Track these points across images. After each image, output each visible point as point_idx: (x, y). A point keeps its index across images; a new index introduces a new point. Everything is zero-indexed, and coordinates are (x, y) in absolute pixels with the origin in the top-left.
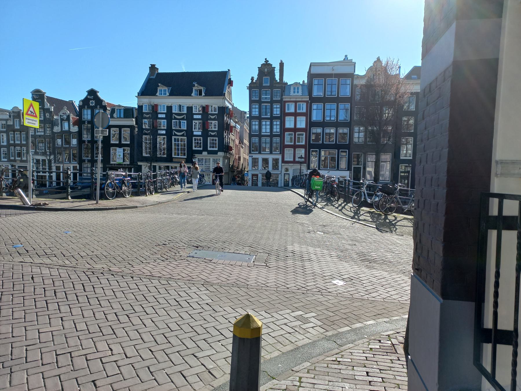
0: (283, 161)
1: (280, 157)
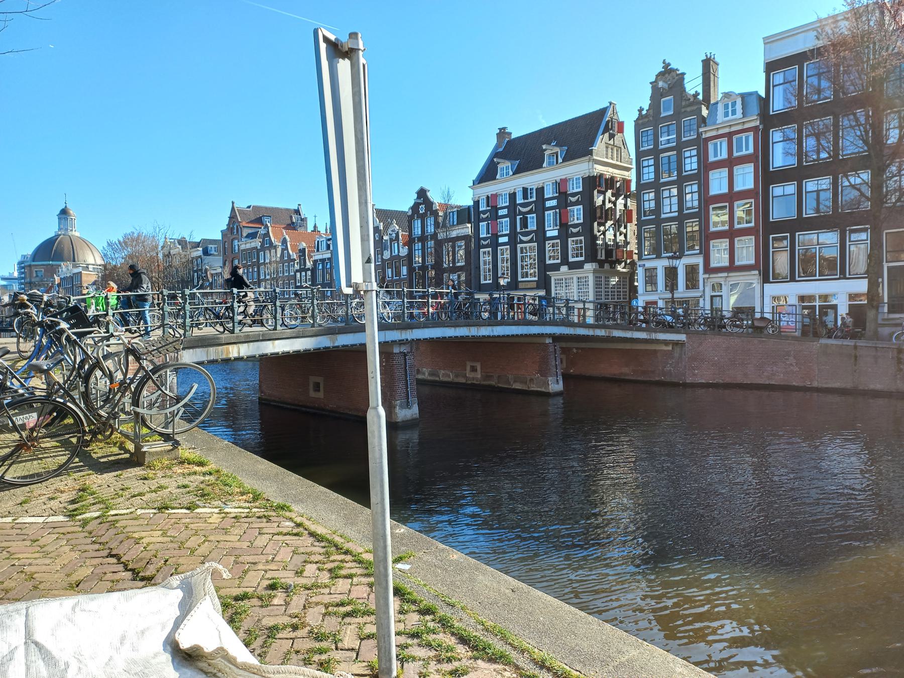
0: (708, 270)
1: (699, 260)
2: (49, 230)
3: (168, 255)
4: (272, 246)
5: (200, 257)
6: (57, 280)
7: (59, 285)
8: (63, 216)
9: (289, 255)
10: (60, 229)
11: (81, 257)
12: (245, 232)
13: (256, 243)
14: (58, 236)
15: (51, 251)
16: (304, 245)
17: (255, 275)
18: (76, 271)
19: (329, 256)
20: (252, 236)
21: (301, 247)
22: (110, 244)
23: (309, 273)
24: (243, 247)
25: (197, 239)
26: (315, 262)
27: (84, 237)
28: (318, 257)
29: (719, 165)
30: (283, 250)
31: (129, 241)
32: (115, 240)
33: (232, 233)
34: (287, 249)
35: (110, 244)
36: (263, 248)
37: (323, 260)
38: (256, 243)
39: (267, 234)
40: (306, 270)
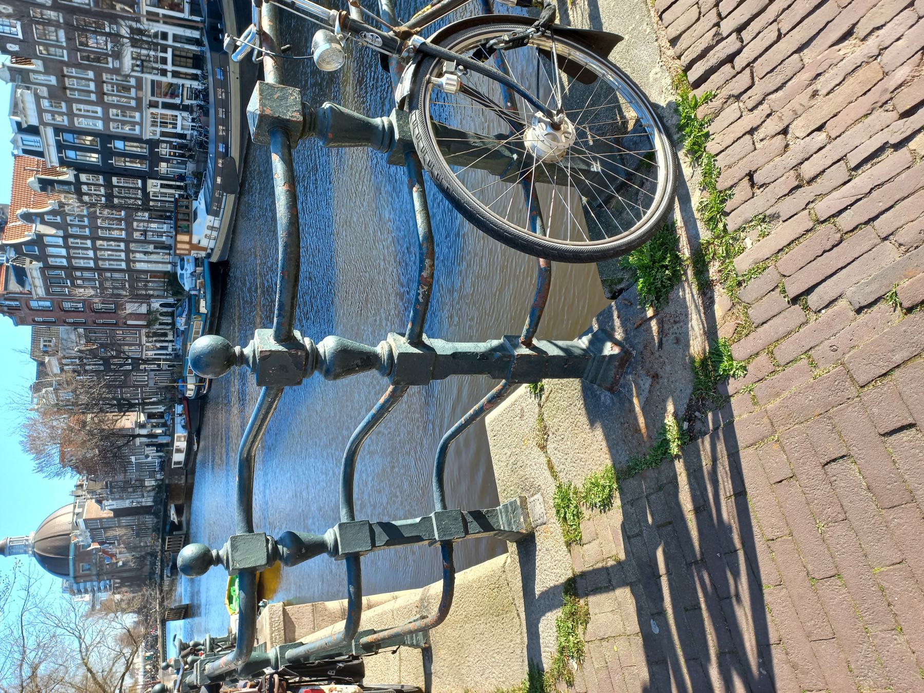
2: (30, 564)
3: (59, 408)
4: (39, 239)
5: (59, 360)
6: (95, 546)
7: (101, 543)
8: (7, 551)
9: (53, 213)
10: (25, 552)
11: (64, 528)
12: (14, 286)
13: (33, 268)
14: (34, 554)
15: (55, 557)
16: (32, 179)
17: (87, 274)
18: (82, 525)
19: (50, 132)
20: (21, 275)
21: (37, 186)
22: (40, 469)
23: (83, 177)
24: (41, 292)
25: (33, 367)
26: (63, 162)
27: (36, 528)
28: (53, 157)
29: (71, 121)
30: (43, 222)
31: (34, 446)
32: (33, 464)
33: (17, 309)
34: (41, 215)
35: (40, 469)
36: (42, 257)
37: (60, 147)
38: (33, 268)
39: (17, 247)
40: (78, 183)
